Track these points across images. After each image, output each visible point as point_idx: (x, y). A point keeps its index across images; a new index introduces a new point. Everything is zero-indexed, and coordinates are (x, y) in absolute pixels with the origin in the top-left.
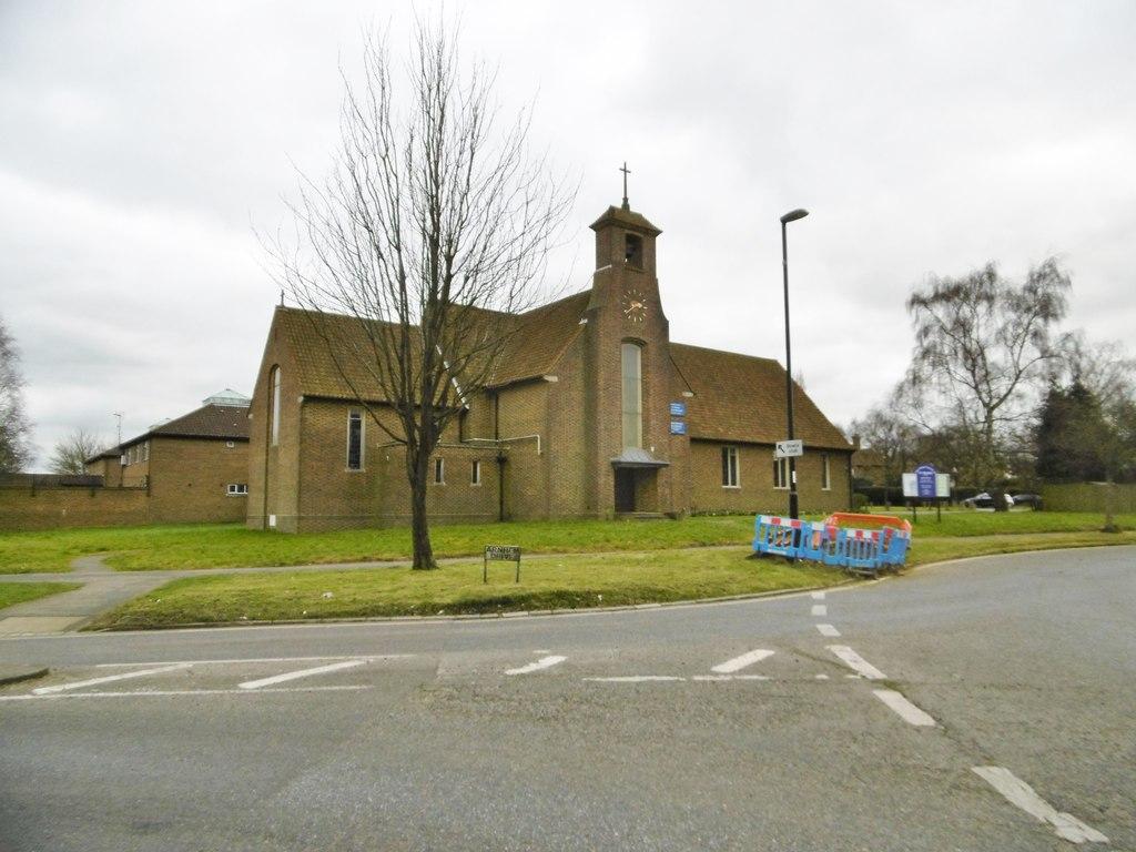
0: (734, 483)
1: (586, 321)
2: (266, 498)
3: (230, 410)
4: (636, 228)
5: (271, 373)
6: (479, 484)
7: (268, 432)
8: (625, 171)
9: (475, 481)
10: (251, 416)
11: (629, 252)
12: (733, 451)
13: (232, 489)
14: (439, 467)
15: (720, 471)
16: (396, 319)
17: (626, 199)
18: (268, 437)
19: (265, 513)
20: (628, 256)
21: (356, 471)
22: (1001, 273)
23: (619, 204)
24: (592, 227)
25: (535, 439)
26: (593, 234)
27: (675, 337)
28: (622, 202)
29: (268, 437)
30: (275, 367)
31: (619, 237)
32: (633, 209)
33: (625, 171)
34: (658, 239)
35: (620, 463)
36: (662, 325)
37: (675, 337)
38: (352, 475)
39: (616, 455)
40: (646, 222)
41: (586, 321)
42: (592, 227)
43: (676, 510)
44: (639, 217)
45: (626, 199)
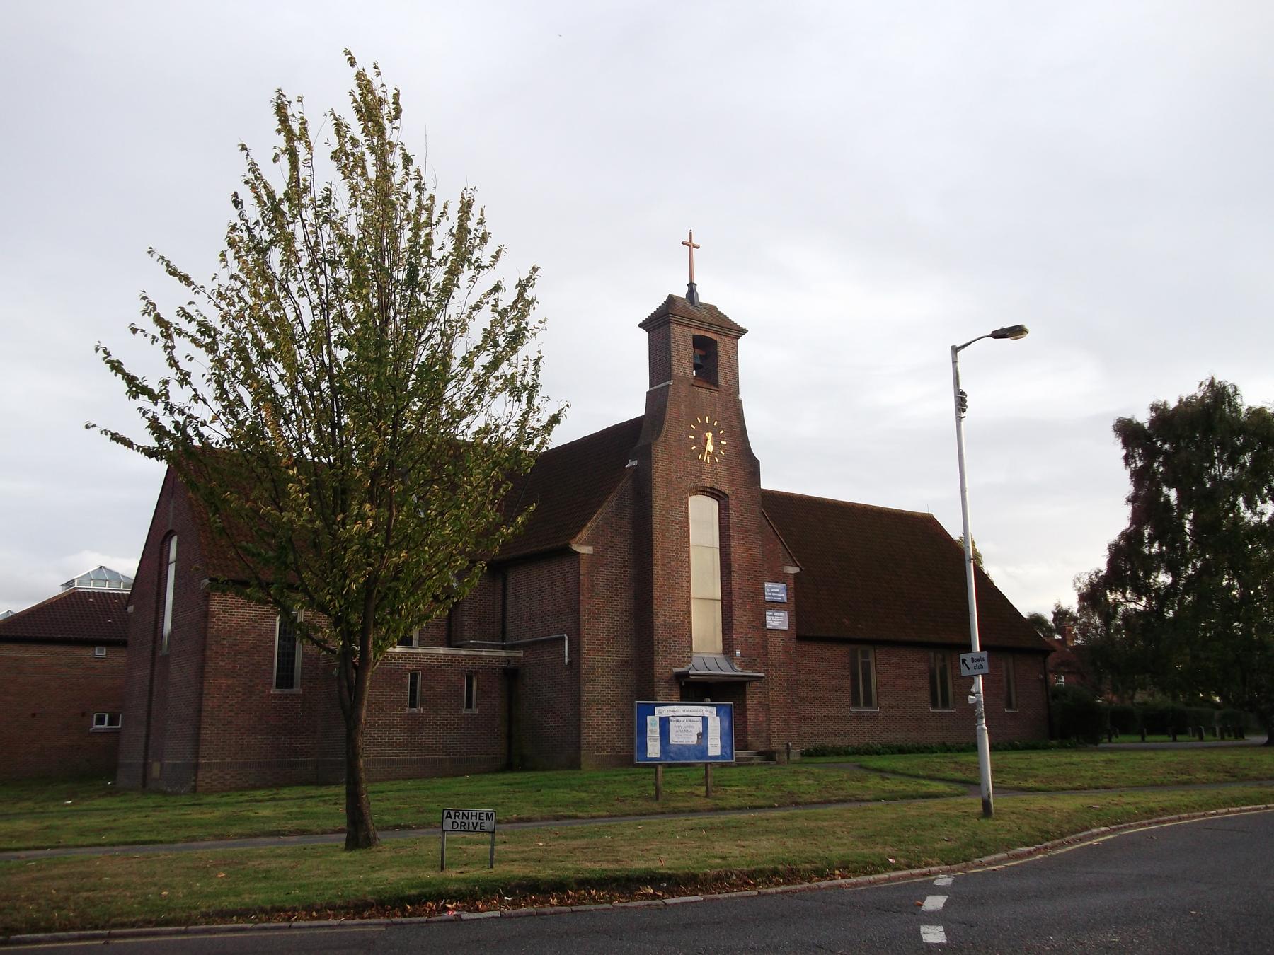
0: (868, 703)
1: (635, 463)
2: (148, 736)
3: (104, 599)
4: (709, 326)
5: (163, 543)
6: (475, 710)
7: (156, 628)
8: (690, 245)
9: (469, 705)
10: (131, 609)
11: (698, 362)
12: (865, 655)
13: (100, 720)
14: (413, 684)
15: (847, 683)
16: (344, 836)
17: (691, 285)
18: (155, 642)
19: (146, 759)
20: (696, 367)
21: (287, 691)
22: (1065, 606)
23: (682, 293)
24: (641, 325)
25: (563, 639)
26: (644, 335)
27: (767, 484)
28: (686, 290)
29: (155, 642)
30: (169, 536)
31: (681, 338)
32: (704, 297)
33: (690, 245)
34: (742, 342)
35: (687, 675)
36: (753, 466)
37: (770, 481)
38: (280, 697)
39: (681, 664)
40: (725, 318)
41: (635, 463)
42: (641, 325)
43: (776, 745)
44: (712, 309)
45: (691, 285)
